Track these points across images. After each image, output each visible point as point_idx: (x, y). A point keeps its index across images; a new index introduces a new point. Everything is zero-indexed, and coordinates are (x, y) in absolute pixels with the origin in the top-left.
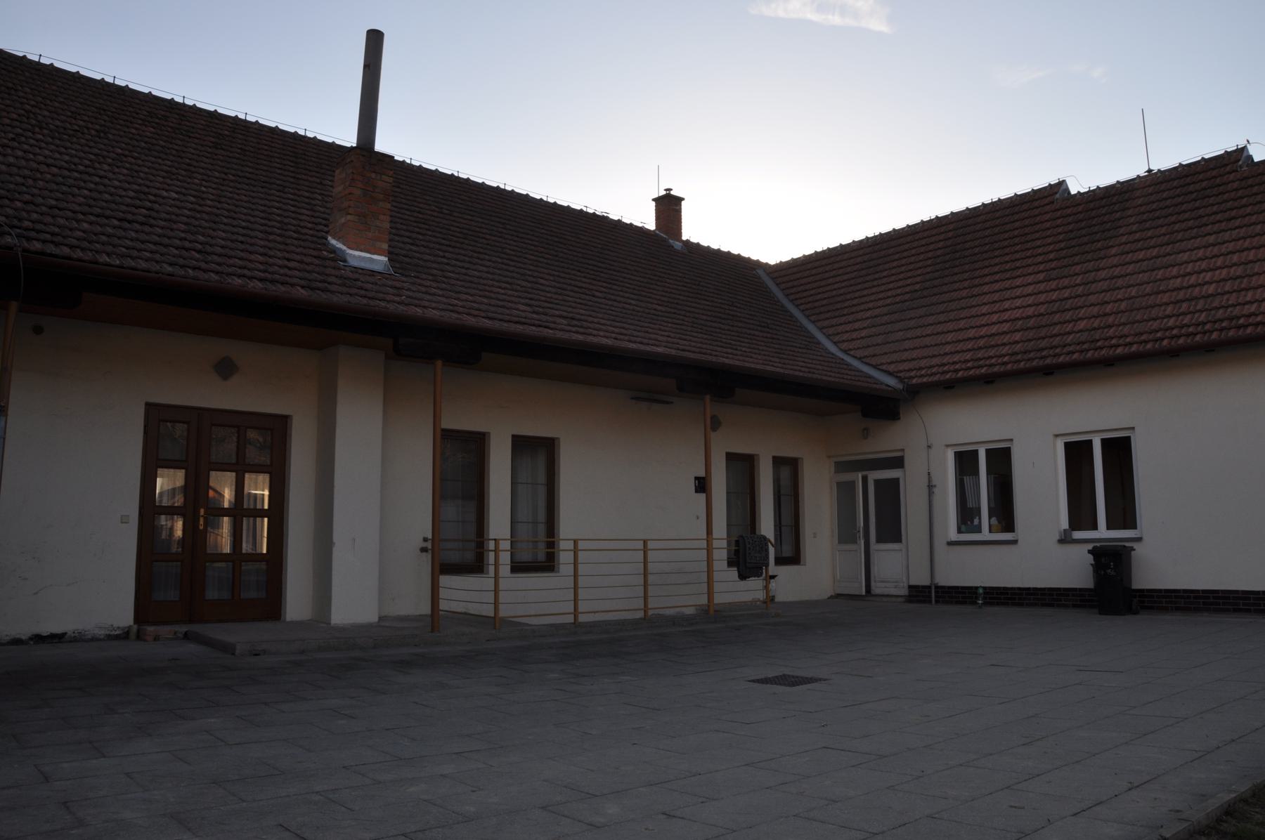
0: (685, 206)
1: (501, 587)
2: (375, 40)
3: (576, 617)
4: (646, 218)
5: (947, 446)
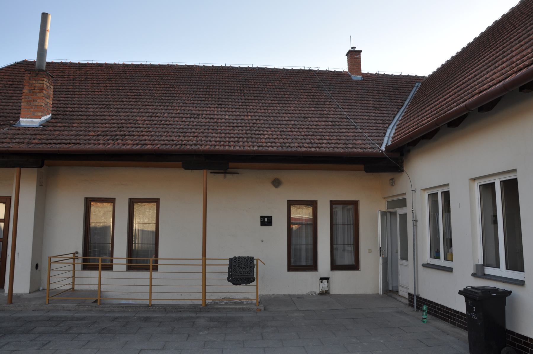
0: (362, 54)
1: (97, 280)
2: (45, 16)
3: (150, 302)
4: (341, 65)
5: (425, 190)
